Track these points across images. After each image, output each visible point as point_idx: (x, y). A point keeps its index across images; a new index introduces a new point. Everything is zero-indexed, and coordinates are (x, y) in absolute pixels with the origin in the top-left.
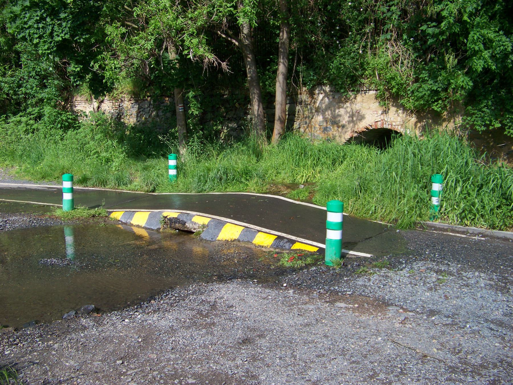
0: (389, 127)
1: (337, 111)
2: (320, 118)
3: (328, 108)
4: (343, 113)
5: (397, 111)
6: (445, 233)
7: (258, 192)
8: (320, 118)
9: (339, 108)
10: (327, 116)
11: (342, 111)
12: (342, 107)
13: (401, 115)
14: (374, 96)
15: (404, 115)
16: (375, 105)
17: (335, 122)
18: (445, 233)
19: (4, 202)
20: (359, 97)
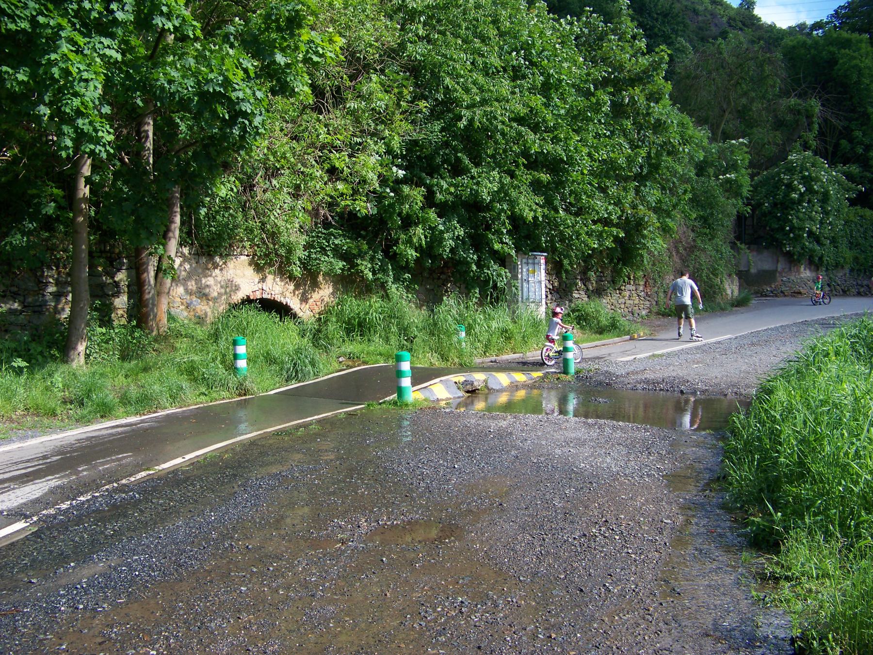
0: (269, 297)
1: (203, 281)
2: (181, 290)
3: (189, 277)
4: (214, 281)
5: (274, 279)
6: (143, 474)
7: (240, 395)
8: (181, 290)
9: (206, 276)
10: (190, 287)
11: (210, 281)
12: (211, 276)
13: (279, 283)
14: (247, 262)
15: (283, 284)
16: (250, 271)
17: (202, 294)
18: (143, 474)
19: (306, 426)
20: (231, 264)
